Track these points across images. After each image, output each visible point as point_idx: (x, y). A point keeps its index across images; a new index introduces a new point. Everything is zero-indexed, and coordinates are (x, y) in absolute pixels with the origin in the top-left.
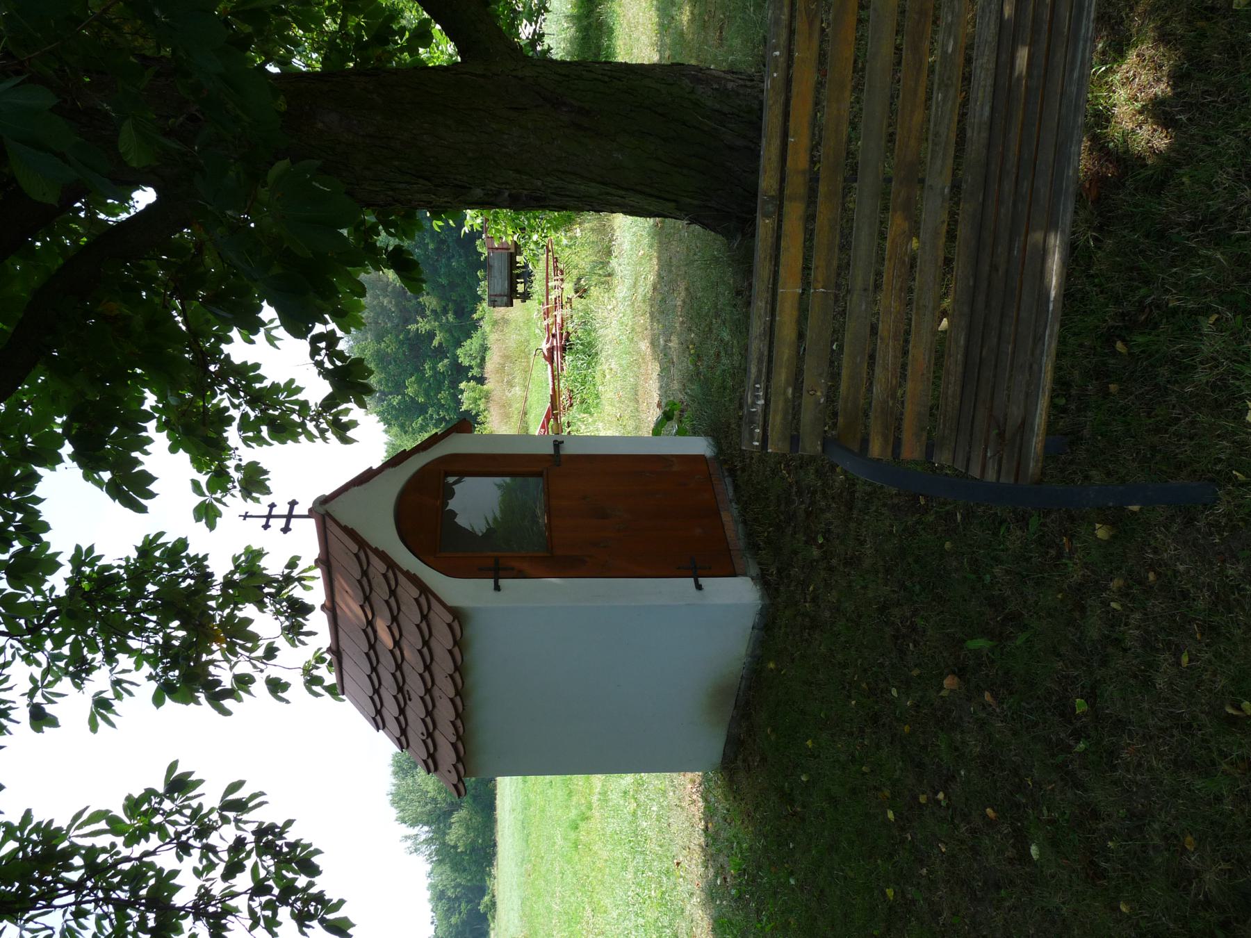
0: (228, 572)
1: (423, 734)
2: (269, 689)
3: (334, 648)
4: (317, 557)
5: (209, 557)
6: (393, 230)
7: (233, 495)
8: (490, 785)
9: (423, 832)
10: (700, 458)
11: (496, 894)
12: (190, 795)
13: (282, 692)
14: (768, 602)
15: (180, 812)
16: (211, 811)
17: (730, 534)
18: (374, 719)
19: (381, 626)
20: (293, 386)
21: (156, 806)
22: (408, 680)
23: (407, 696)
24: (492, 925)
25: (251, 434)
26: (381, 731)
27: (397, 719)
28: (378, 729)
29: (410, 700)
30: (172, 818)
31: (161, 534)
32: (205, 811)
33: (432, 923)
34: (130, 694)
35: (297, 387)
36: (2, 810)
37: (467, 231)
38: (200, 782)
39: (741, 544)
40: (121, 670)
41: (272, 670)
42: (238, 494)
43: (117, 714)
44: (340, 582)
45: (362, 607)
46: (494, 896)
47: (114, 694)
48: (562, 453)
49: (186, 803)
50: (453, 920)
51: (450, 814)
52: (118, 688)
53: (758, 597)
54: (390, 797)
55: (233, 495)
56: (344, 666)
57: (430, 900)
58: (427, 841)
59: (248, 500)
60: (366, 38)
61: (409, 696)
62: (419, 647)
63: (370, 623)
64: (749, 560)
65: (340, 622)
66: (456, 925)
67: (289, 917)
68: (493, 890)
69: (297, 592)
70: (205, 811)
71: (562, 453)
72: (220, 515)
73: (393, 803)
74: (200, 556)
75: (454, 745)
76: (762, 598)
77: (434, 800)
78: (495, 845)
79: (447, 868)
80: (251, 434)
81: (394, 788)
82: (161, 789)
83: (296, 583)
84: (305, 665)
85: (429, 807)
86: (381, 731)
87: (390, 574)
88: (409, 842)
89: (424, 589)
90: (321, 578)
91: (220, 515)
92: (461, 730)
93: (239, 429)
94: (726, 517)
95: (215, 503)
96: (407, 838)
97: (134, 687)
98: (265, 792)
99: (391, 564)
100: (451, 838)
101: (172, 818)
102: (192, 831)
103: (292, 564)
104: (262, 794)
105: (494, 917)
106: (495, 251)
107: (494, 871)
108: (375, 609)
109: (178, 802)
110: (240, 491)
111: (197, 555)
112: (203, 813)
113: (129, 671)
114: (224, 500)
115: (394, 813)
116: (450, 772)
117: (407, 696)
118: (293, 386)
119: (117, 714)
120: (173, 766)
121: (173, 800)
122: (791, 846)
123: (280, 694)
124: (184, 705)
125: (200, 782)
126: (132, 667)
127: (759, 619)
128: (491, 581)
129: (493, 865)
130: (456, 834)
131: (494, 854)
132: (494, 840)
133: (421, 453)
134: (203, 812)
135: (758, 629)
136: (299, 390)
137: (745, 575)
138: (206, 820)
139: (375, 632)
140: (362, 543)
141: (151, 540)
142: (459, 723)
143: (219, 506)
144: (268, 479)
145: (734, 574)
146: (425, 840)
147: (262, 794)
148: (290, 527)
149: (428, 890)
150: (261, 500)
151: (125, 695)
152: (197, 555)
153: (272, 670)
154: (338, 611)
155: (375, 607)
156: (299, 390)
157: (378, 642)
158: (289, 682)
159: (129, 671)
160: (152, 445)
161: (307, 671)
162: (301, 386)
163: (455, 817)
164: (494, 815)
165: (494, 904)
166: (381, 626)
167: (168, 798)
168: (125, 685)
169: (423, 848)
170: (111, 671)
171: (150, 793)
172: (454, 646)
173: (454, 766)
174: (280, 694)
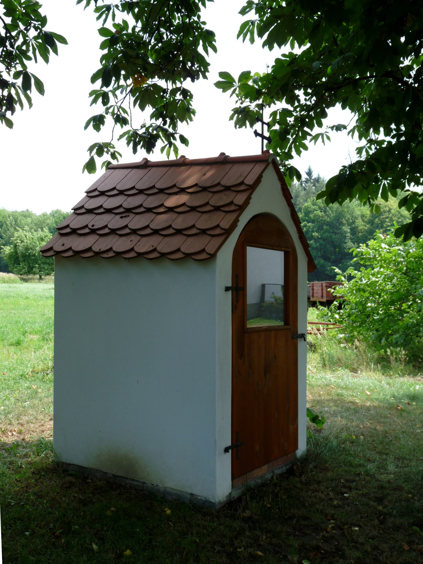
0: (192, 93)
1: (93, 226)
2: (97, 116)
3: (149, 164)
4: (187, 157)
5: (206, 80)
7: (237, 102)
10: (296, 447)
12: (37, 52)
13: (93, 125)
14: (218, 507)
15: (25, 42)
16: (24, 66)
18: (96, 190)
19: (183, 198)
20: (301, 149)
21: (32, 25)
22: (138, 217)
23: (124, 215)
25: (278, 117)
26: (86, 194)
27: (101, 207)
28: (87, 192)
29: (121, 217)
30: (21, 37)
31: (215, 49)
32: (25, 61)
34: (98, 18)
35: (301, 152)
37: (336, 271)
38: (47, 60)
39: (252, 483)
40: (115, 13)
41: (109, 120)
42: (238, 105)
43: (85, 7)
44: (211, 172)
45: (196, 185)
47: (99, 7)
48: (299, 339)
49: (31, 48)
52: (105, 9)
55: (237, 102)
56: (135, 170)
59: (233, 112)
61: (125, 217)
62: (71, 226)
63: (183, 191)
64: (241, 490)
65: (173, 169)
67: (33, 106)
69: (160, 143)
70: (25, 61)
72: (224, 91)
74: (207, 74)
75: (89, 249)
76: (220, 503)
80: (278, 117)
82: (47, 29)
83: (166, 143)
84: (112, 144)
86: (86, 194)
87: (233, 208)
89: (228, 232)
90: (167, 159)
91: (224, 91)
92: (105, 255)
93: (284, 110)
94: (265, 468)
95: (233, 89)
97: (102, 22)
98: (32, 108)
99: (242, 208)
101: (21, 37)
102: (11, 49)
103: (184, 140)
104: (31, 105)
106: (311, 288)
108: (196, 194)
109: (34, 42)
110: (240, 107)
111: (208, 72)
112: (24, 59)
113: (114, 19)
114: (234, 95)
116: (63, 245)
117: (124, 215)
118: (301, 149)
119: (85, 7)
120: (63, 41)
121: (35, 38)
122: (27, 533)
123: (92, 123)
125: (47, 60)
126: (117, 22)
127: (201, 500)
128: (230, 284)
133: (297, 235)
134: (24, 60)
135: (190, 498)
136: (299, 153)
138: (18, 61)
139: (176, 193)
140: (253, 187)
141: (211, 42)
142: (111, 254)
143: (230, 91)
144: (246, 127)
147: (31, 105)
148: (258, 137)
150: (231, 121)
151: (98, 14)
152: (208, 72)
153: (109, 120)
154: (183, 168)
155: (199, 195)
156: (299, 153)
157: (167, 196)
158: (100, 131)
159: (114, 19)
160: (268, 49)
161: (108, 145)
162: (301, 155)
166: (183, 198)
167: (39, 34)
168: (104, 16)
170: (117, 6)
171: (44, 21)
172: (136, 253)
173: (70, 249)
174: (92, 123)
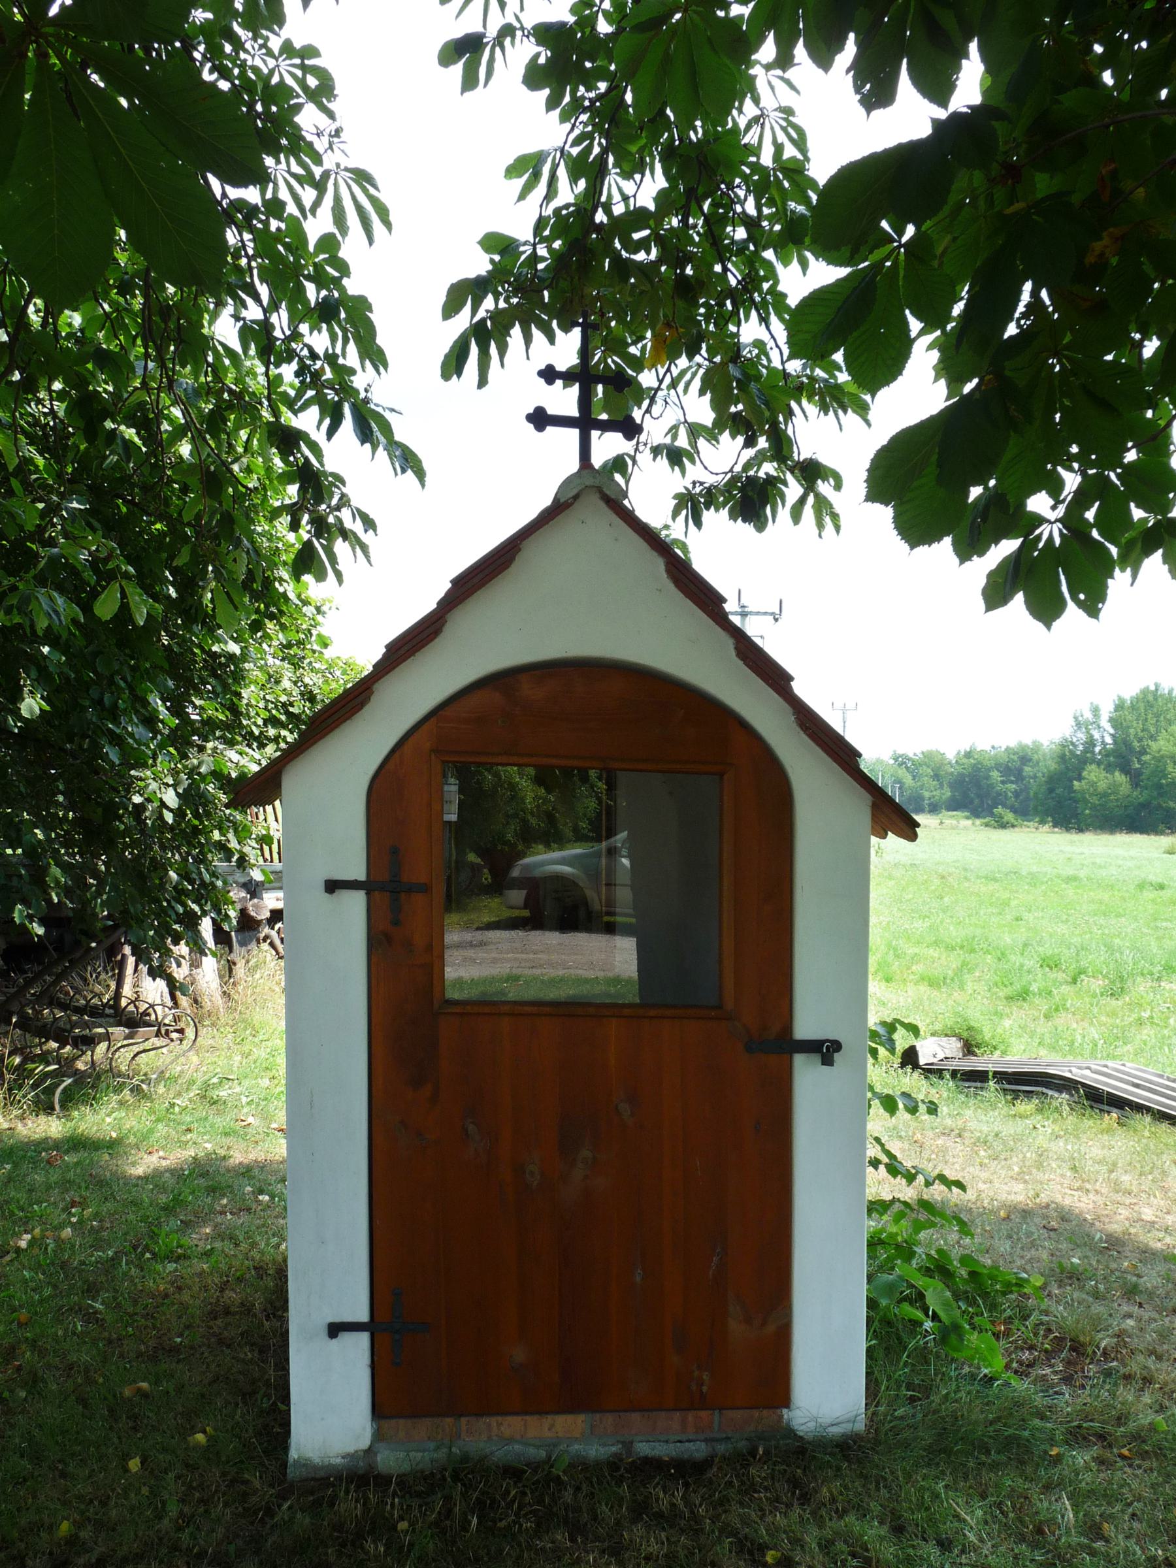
6: (1082, 597)
8: (1161, 827)
9: (1105, 735)
11: (1016, 829)
17: (511, 1425)
24: (978, 822)
33: (993, 747)
36: (312, 5)
46: (1013, 826)
50: (995, 774)
51: (1126, 769)
53: (310, 1454)
54: (1152, 688)
57: (1020, 744)
58: (1091, 743)
60: (884, 224)
66: (988, 777)
68: (1021, 826)
71: (799, 1060)
73: (1145, 691)
77: (1143, 752)
78: (1081, 830)
79: (1053, 766)
81: (1166, 692)
85: (1136, 744)
88: (1088, 715)
96: (1096, 711)
100: (1093, 774)
105: (987, 825)
107: (1046, 828)
115: (1129, 692)
124: (454, 281)
128: (358, 872)
129: (1054, 826)
130: (1096, 777)
131: (1068, 829)
132: (1087, 829)
137: (379, 1436)
145: (378, 1411)
146: (1092, 736)
149: (1034, 742)
163: (1119, 777)
164: (1121, 831)
165: (1003, 826)
169: (1081, 736)
